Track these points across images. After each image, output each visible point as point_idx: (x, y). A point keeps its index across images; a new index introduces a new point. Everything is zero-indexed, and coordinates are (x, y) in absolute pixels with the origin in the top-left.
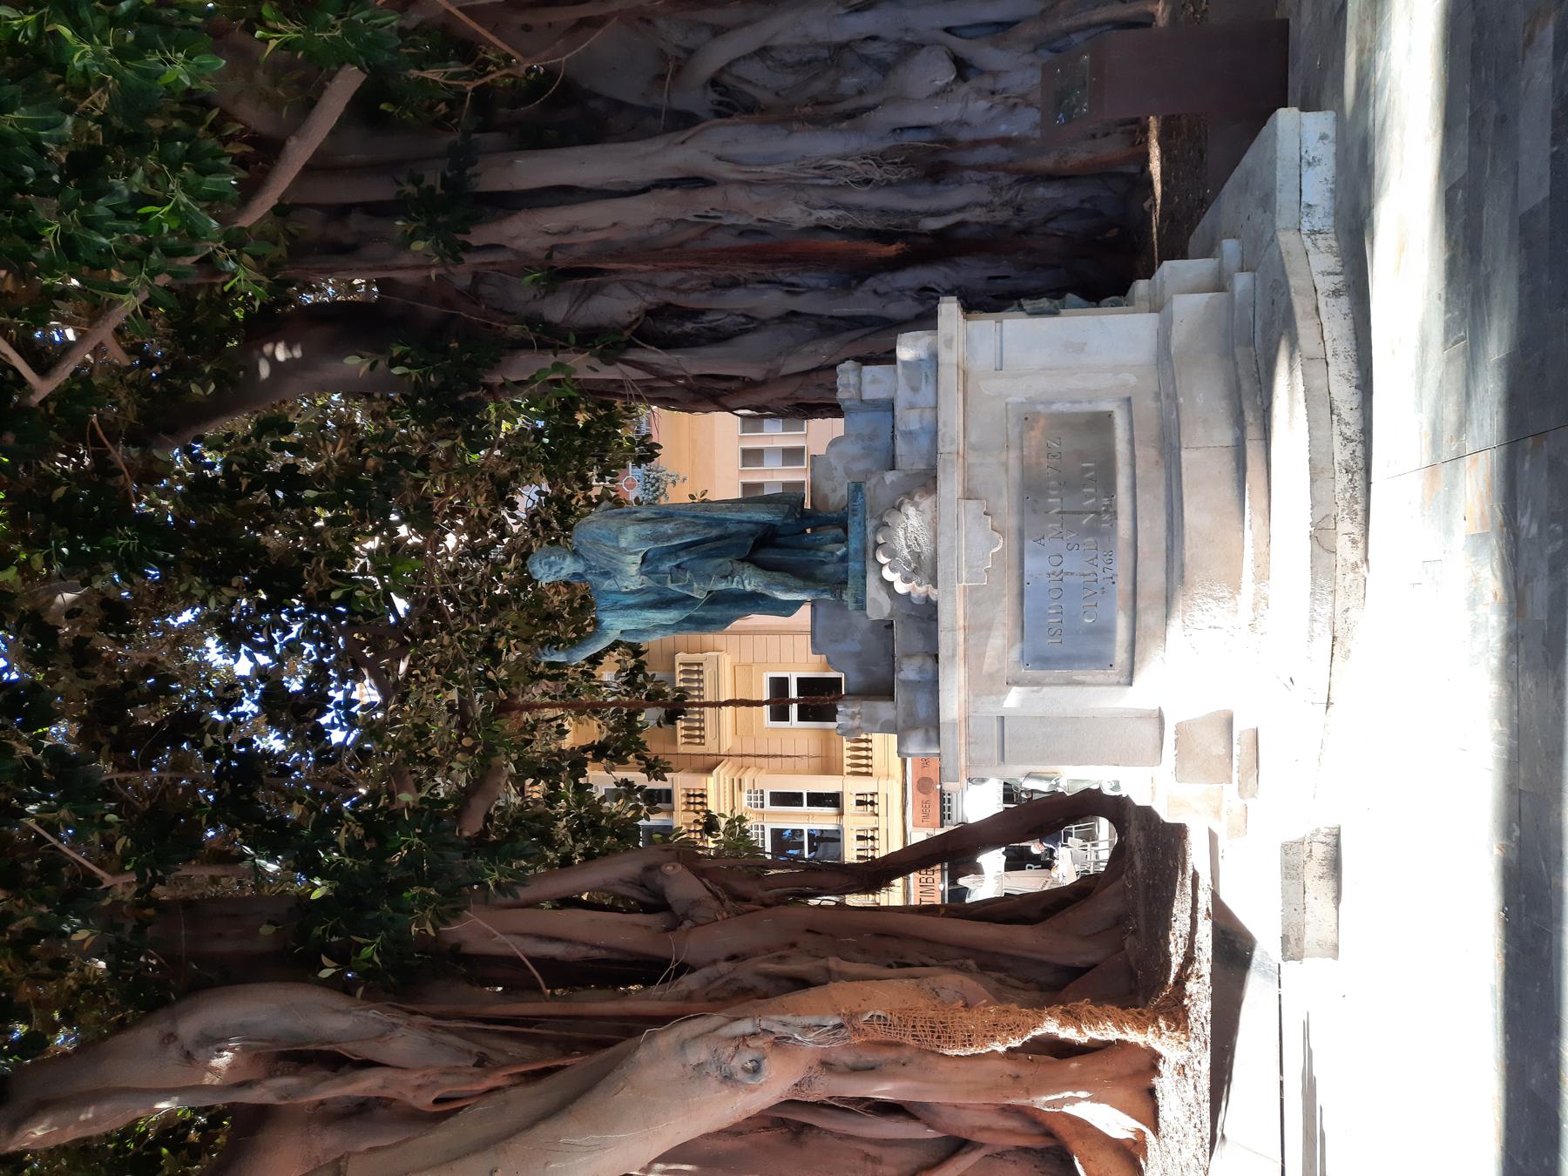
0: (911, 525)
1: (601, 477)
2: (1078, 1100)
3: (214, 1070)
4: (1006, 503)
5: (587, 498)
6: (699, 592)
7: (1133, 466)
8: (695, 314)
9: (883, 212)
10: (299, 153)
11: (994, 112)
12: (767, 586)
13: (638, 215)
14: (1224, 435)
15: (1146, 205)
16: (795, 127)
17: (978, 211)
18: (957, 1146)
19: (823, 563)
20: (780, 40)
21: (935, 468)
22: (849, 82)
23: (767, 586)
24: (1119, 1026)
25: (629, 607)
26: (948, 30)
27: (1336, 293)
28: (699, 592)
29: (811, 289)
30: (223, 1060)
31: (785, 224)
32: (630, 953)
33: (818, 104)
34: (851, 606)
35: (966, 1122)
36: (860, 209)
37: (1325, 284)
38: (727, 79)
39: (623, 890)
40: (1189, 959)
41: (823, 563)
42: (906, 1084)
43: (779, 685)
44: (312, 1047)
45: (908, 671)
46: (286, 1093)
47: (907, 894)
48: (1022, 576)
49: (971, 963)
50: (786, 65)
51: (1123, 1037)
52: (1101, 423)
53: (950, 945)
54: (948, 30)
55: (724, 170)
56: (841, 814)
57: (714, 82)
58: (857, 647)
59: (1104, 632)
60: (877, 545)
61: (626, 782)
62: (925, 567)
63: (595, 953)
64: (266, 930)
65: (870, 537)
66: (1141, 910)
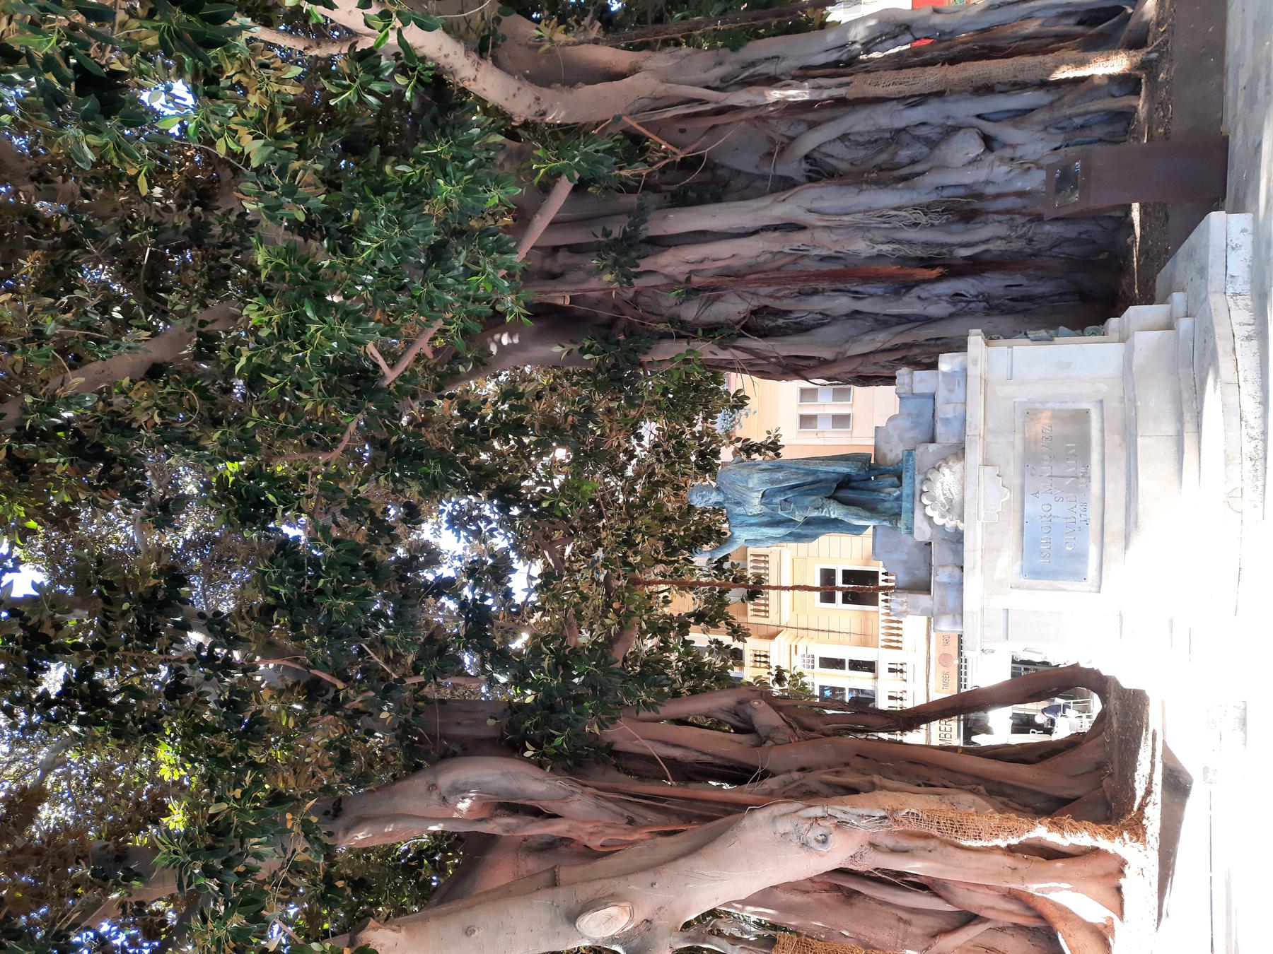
0: (946, 481)
1: (705, 420)
2: (1062, 889)
3: (459, 811)
4: (1012, 470)
5: (693, 434)
6: (799, 517)
7: (1103, 446)
8: (787, 313)
9: (926, 244)
10: (540, 224)
11: (1013, 174)
12: (846, 515)
13: (749, 250)
14: (1170, 428)
15: (1129, 240)
16: (864, 187)
17: (999, 242)
18: (969, 918)
19: (884, 501)
20: (856, 129)
21: (964, 442)
22: (904, 154)
23: (846, 515)
24: (1094, 835)
25: (752, 525)
26: (979, 116)
27: (1249, 338)
28: (799, 517)
29: (871, 295)
30: (464, 805)
31: (855, 254)
32: (728, 760)
33: (881, 170)
34: (903, 531)
35: (977, 901)
36: (910, 242)
37: (1241, 332)
38: (816, 155)
39: (722, 716)
40: (1149, 792)
41: (884, 501)
42: (932, 865)
43: (828, 575)
44: (520, 802)
45: (941, 576)
46: (508, 829)
47: (928, 736)
48: (1023, 511)
49: (982, 788)
50: (858, 144)
51: (1096, 844)
52: (1081, 417)
53: (965, 774)
54: (979, 116)
55: (812, 219)
56: (876, 678)
57: (807, 157)
58: (904, 557)
59: (1081, 556)
60: (922, 492)
61: (717, 642)
62: (957, 508)
63: (703, 758)
64: (491, 722)
65: (918, 486)
66: (1116, 758)
